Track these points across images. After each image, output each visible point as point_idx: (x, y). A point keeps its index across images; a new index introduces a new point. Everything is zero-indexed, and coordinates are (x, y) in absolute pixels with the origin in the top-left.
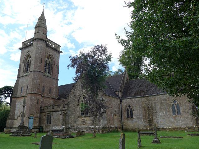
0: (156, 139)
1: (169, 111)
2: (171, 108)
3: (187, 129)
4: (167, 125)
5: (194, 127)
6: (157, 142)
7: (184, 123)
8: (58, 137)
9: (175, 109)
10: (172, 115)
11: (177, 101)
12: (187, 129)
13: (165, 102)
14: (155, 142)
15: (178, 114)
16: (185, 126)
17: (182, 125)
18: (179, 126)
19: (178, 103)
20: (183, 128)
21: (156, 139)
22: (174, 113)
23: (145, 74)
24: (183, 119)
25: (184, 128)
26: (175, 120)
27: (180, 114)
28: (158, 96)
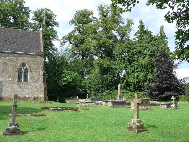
0: (13, 127)
1: (14, 76)
2: (17, 73)
3: (32, 99)
4: (8, 93)
5: (41, 97)
6: (14, 132)
7: (30, 92)
8: (50, 35)
9: (22, 74)
10: (17, 81)
11: (27, 65)
12: (32, 99)
13: (10, 63)
14: (10, 132)
15: (24, 81)
16: (30, 96)
17: (27, 94)
18: (23, 96)
19: (28, 68)
20: (27, 98)
21: (13, 127)
22: (20, 79)
23: (119, 13)
24: (29, 87)
25: (28, 98)
26: (20, 87)
27: (27, 81)
28: (3, 54)
